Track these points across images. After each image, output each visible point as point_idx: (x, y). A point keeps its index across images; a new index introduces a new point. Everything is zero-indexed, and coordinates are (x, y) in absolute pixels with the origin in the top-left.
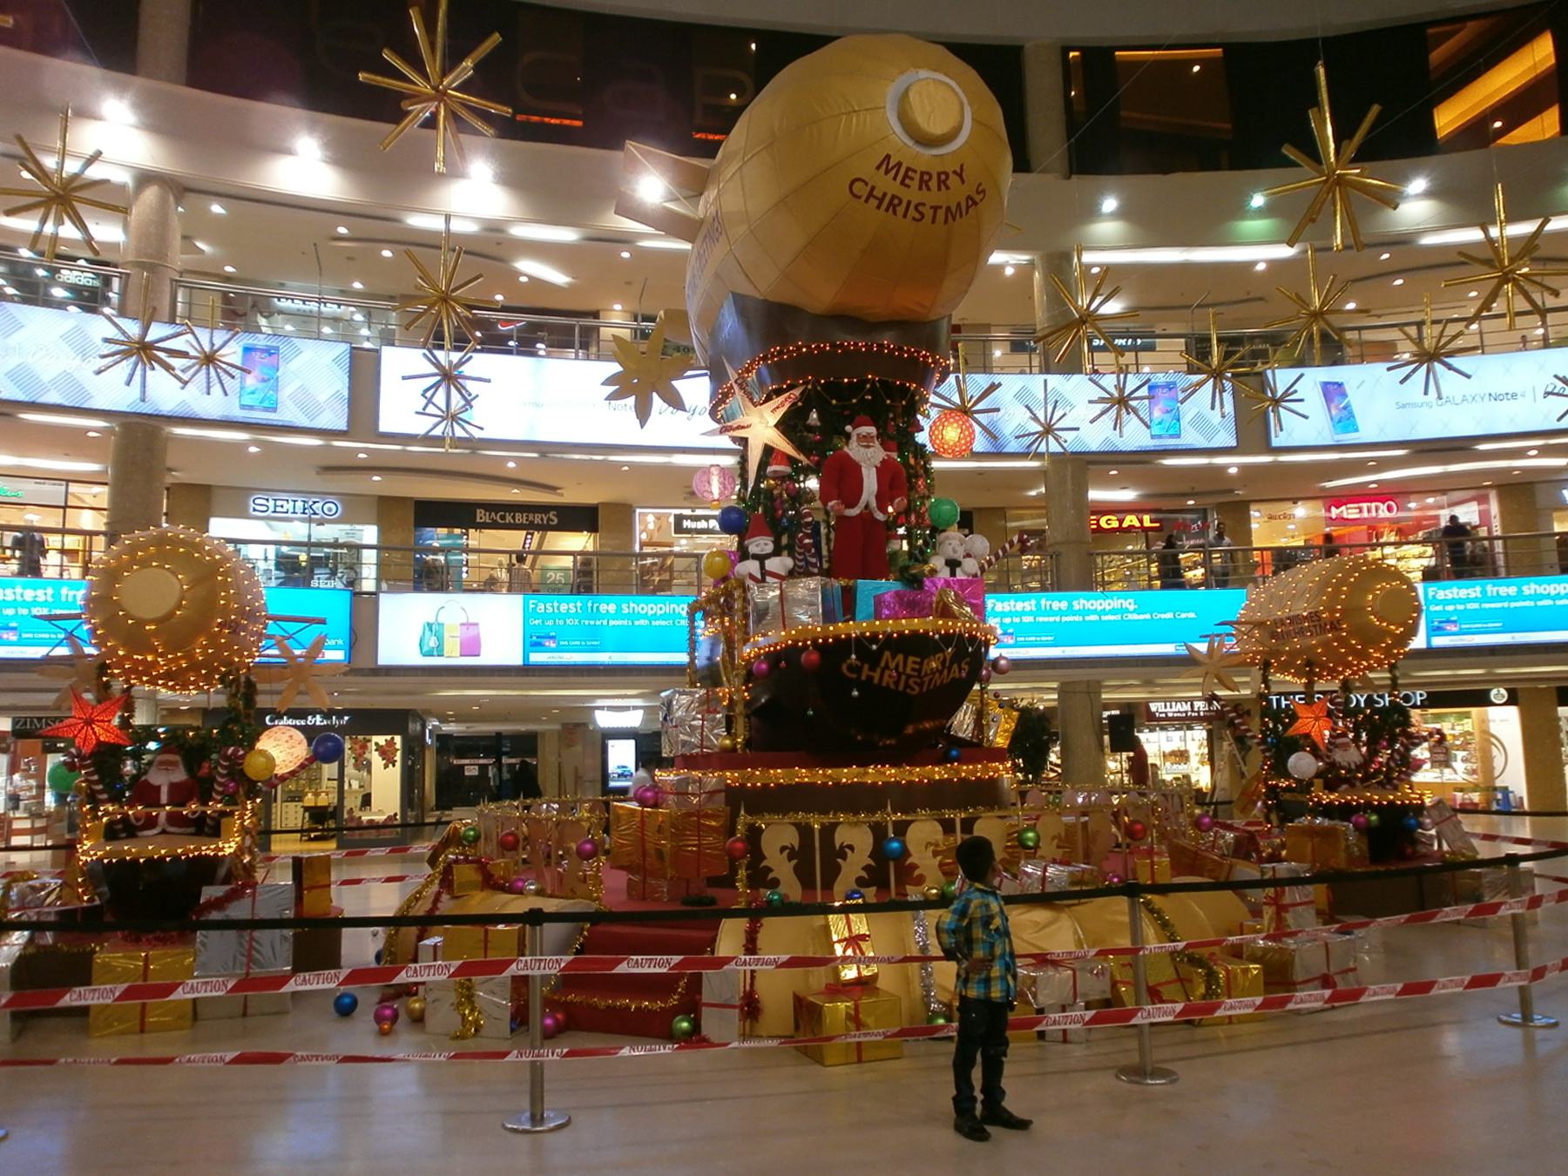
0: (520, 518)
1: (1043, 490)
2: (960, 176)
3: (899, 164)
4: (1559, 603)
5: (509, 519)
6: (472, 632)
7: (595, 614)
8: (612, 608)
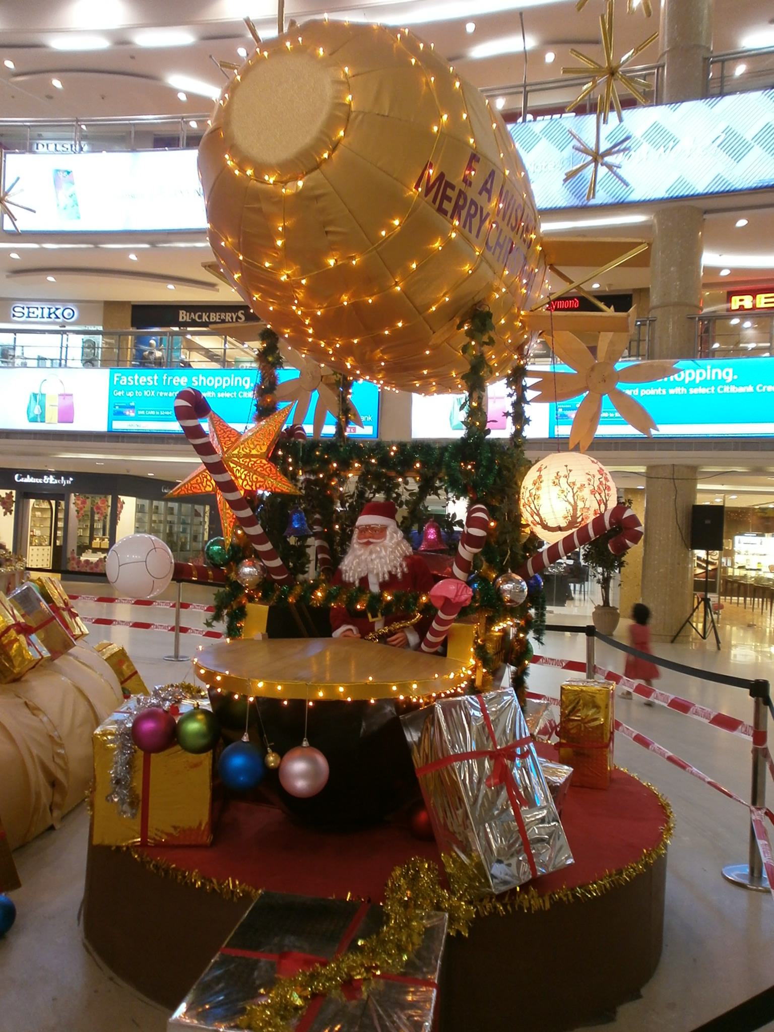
0: (214, 317)
1: (710, 258)
4: (692, 391)
5: (205, 318)
6: (67, 401)
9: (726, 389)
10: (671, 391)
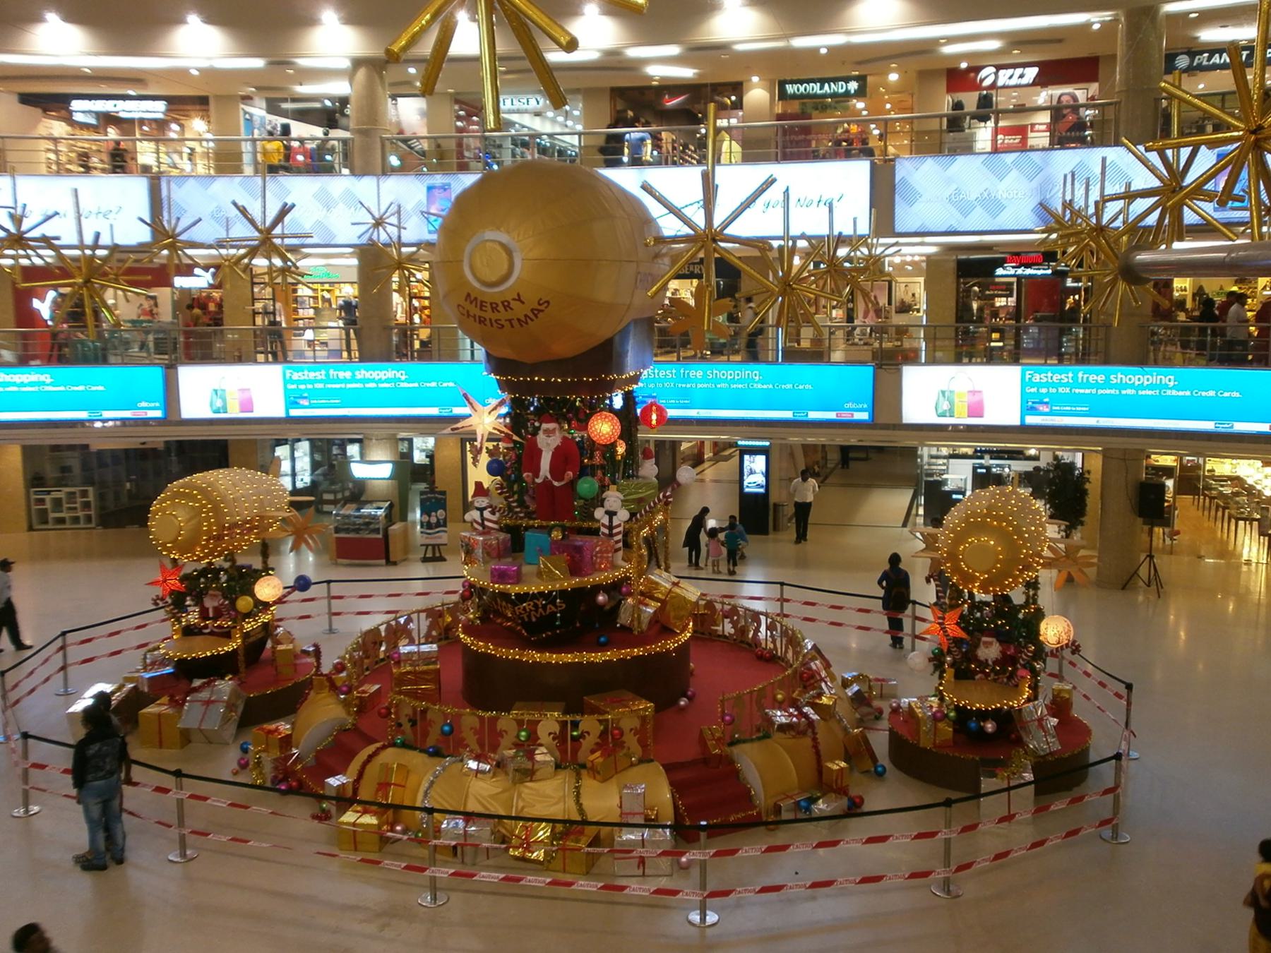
2: (519, 299)
3: (526, 316)
4: (381, 385)
6: (976, 398)
7: (686, 378)
8: (699, 374)
9: (1169, 392)
10: (1124, 392)
